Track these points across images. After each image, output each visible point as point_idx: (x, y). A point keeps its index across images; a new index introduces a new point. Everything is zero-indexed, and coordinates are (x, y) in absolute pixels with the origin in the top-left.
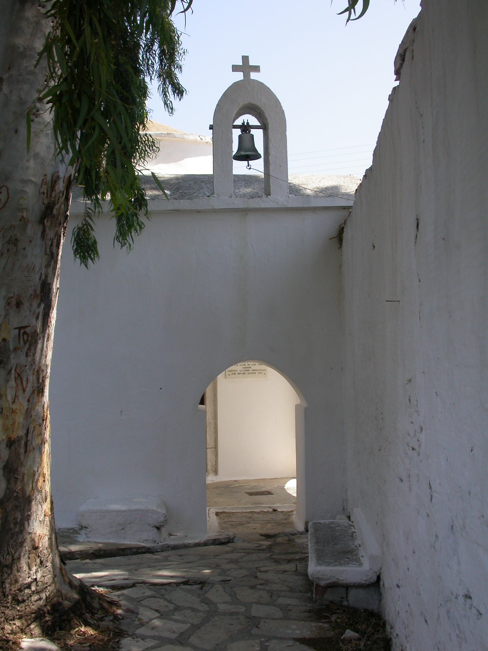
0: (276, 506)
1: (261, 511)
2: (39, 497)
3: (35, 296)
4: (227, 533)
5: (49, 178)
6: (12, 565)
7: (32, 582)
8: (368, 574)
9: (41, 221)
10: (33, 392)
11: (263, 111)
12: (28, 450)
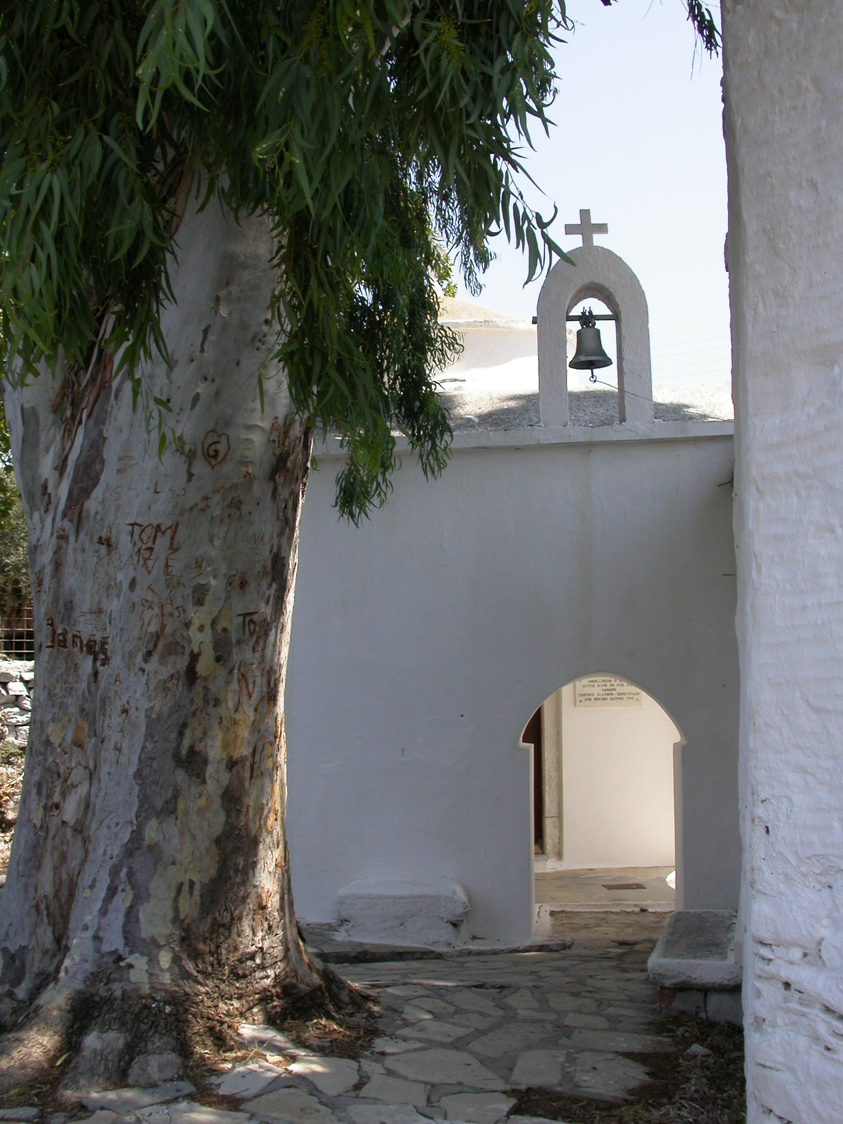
0: (644, 903)
1: (622, 912)
2: (268, 840)
3: (265, 573)
4: (561, 938)
5: (281, 421)
6: (230, 926)
7: (256, 952)
8: (733, 970)
9: (272, 477)
10: (262, 699)
11: (612, 294)
12: (254, 775)
